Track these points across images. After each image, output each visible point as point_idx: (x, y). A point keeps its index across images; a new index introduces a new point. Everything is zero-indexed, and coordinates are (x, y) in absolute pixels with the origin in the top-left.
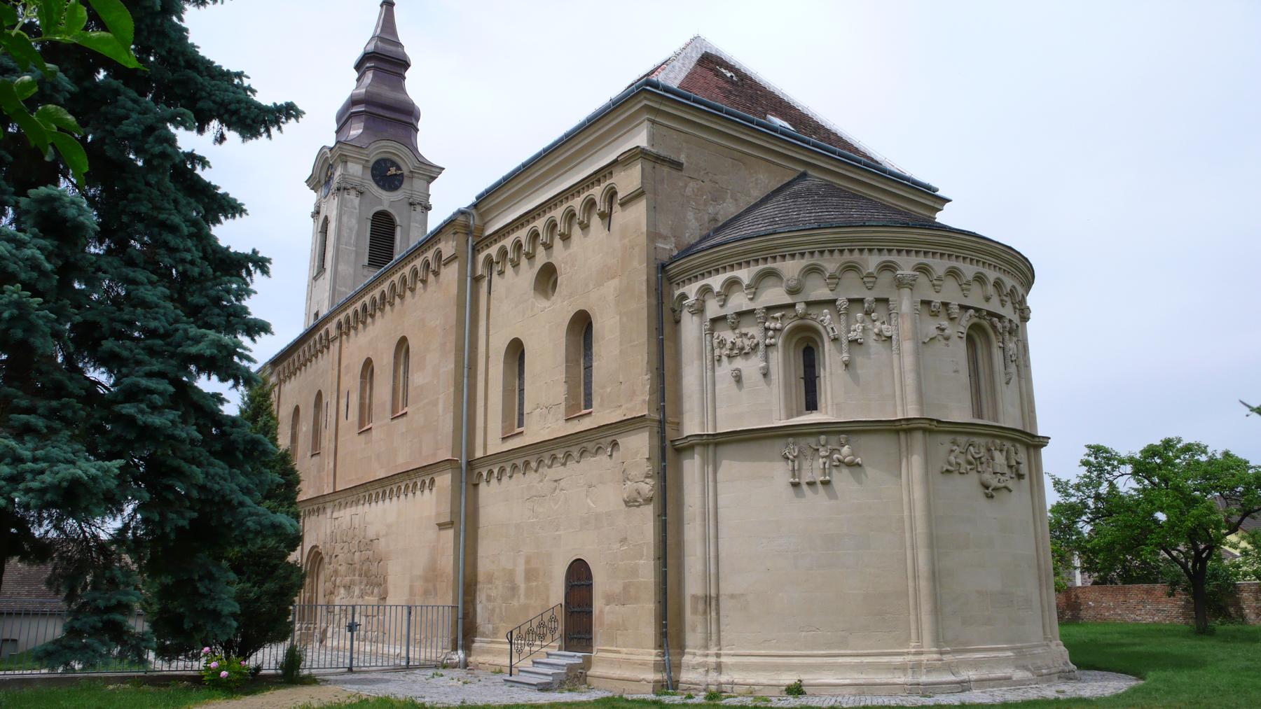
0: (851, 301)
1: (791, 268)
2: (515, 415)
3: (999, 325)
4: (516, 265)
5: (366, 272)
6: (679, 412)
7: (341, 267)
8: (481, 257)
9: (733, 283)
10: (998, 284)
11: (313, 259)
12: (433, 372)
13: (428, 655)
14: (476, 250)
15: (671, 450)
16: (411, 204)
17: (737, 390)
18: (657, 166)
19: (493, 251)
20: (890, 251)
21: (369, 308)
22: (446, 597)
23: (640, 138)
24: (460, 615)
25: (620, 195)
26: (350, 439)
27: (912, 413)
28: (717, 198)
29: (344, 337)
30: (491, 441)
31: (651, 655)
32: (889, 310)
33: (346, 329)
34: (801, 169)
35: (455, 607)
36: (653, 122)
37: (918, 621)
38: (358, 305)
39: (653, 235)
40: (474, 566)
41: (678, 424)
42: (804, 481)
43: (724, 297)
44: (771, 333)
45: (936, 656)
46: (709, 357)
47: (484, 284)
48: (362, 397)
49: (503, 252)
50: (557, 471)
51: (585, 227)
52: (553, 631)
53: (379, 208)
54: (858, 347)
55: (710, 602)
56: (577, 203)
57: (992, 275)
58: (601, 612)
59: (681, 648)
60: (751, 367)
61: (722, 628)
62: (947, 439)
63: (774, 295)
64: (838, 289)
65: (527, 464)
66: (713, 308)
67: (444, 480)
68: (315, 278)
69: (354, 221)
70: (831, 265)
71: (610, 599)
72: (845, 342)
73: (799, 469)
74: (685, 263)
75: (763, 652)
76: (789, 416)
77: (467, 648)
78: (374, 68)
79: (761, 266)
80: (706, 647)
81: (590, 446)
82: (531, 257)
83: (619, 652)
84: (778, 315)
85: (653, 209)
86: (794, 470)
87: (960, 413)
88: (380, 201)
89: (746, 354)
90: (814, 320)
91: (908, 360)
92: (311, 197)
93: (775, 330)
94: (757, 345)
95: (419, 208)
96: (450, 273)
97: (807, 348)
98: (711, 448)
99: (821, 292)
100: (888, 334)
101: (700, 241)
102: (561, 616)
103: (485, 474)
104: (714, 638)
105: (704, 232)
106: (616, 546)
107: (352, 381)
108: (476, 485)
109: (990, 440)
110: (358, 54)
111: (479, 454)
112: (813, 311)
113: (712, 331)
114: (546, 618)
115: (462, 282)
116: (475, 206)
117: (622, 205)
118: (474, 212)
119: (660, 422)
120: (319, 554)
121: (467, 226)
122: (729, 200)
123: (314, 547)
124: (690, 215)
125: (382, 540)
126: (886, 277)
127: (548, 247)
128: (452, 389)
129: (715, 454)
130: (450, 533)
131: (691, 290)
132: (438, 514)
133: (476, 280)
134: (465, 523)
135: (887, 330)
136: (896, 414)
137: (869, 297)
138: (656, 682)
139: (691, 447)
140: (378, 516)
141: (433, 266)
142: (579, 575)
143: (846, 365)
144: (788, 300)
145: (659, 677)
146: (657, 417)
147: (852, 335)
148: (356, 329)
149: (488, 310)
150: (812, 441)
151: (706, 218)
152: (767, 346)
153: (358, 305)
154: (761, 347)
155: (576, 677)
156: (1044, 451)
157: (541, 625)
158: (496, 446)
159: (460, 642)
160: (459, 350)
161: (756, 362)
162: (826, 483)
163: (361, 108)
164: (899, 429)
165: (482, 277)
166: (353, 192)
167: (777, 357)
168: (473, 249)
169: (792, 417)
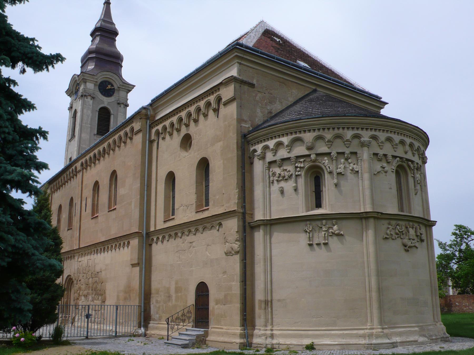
0: (338, 153)
1: (308, 137)
2: (170, 210)
5: (95, 137)
6: (252, 209)
8: (154, 130)
9: (279, 144)
10: (411, 145)
11: (69, 131)
12: (129, 188)
14: (151, 127)
16: (118, 104)
17: (281, 198)
18: (242, 86)
19: (160, 127)
20: (358, 128)
22: (135, 301)
25: (224, 100)
26: (87, 222)
29: (85, 170)
30: (158, 222)
31: (238, 330)
33: (85, 166)
34: (314, 88)
35: (140, 306)
36: (240, 64)
39: (240, 120)
41: (252, 214)
43: (275, 151)
44: (298, 169)
46: (268, 181)
47: (155, 144)
49: (165, 128)
50: (191, 238)
52: (189, 318)
53: (102, 106)
55: (268, 303)
56: (202, 104)
58: (213, 308)
59: (253, 326)
60: (288, 186)
61: (274, 316)
62: (386, 222)
63: (300, 150)
65: (176, 234)
66: (270, 157)
68: (70, 141)
69: (90, 112)
70: (328, 135)
71: (217, 302)
73: (313, 237)
74: (256, 134)
77: (146, 327)
79: (294, 136)
80: (266, 326)
82: (179, 130)
83: (222, 329)
84: (302, 160)
85: (240, 107)
86: (310, 237)
89: (286, 179)
91: (367, 183)
93: (301, 168)
94: (292, 175)
95: (122, 106)
96: (138, 138)
98: (268, 227)
102: (193, 310)
104: (269, 321)
105: (265, 119)
107: (88, 192)
108: (151, 245)
109: (407, 223)
111: (152, 229)
112: (320, 159)
114: (186, 311)
118: (150, 108)
121: (146, 115)
122: (278, 103)
123: (68, 276)
124: (258, 110)
125: (103, 272)
126: (356, 141)
127: (187, 126)
128: (139, 197)
130: (137, 269)
131: (259, 148)
132: (131, 259)
133: (151, 142)
135: (356, 168)
137: (347, 151)
138: (241, 343)
139: (259, 226)
140: (101, 260)
143: (336, 185)
144: (307, 153)
145: (242, 341)
146: (241, 211)
147: (339, 170)
148: (90, 166)
151: (266, 111)
153: (92, 154)
154: (294, 176)
156: (434, 228)
158: (161, 225)
159: (142, 324)
160: (142, 177)
162: (326, 244)
164: (362, 217)
165: (154, 140)
166: (89, 98)
167: (301, 181)
168: (150, 126)
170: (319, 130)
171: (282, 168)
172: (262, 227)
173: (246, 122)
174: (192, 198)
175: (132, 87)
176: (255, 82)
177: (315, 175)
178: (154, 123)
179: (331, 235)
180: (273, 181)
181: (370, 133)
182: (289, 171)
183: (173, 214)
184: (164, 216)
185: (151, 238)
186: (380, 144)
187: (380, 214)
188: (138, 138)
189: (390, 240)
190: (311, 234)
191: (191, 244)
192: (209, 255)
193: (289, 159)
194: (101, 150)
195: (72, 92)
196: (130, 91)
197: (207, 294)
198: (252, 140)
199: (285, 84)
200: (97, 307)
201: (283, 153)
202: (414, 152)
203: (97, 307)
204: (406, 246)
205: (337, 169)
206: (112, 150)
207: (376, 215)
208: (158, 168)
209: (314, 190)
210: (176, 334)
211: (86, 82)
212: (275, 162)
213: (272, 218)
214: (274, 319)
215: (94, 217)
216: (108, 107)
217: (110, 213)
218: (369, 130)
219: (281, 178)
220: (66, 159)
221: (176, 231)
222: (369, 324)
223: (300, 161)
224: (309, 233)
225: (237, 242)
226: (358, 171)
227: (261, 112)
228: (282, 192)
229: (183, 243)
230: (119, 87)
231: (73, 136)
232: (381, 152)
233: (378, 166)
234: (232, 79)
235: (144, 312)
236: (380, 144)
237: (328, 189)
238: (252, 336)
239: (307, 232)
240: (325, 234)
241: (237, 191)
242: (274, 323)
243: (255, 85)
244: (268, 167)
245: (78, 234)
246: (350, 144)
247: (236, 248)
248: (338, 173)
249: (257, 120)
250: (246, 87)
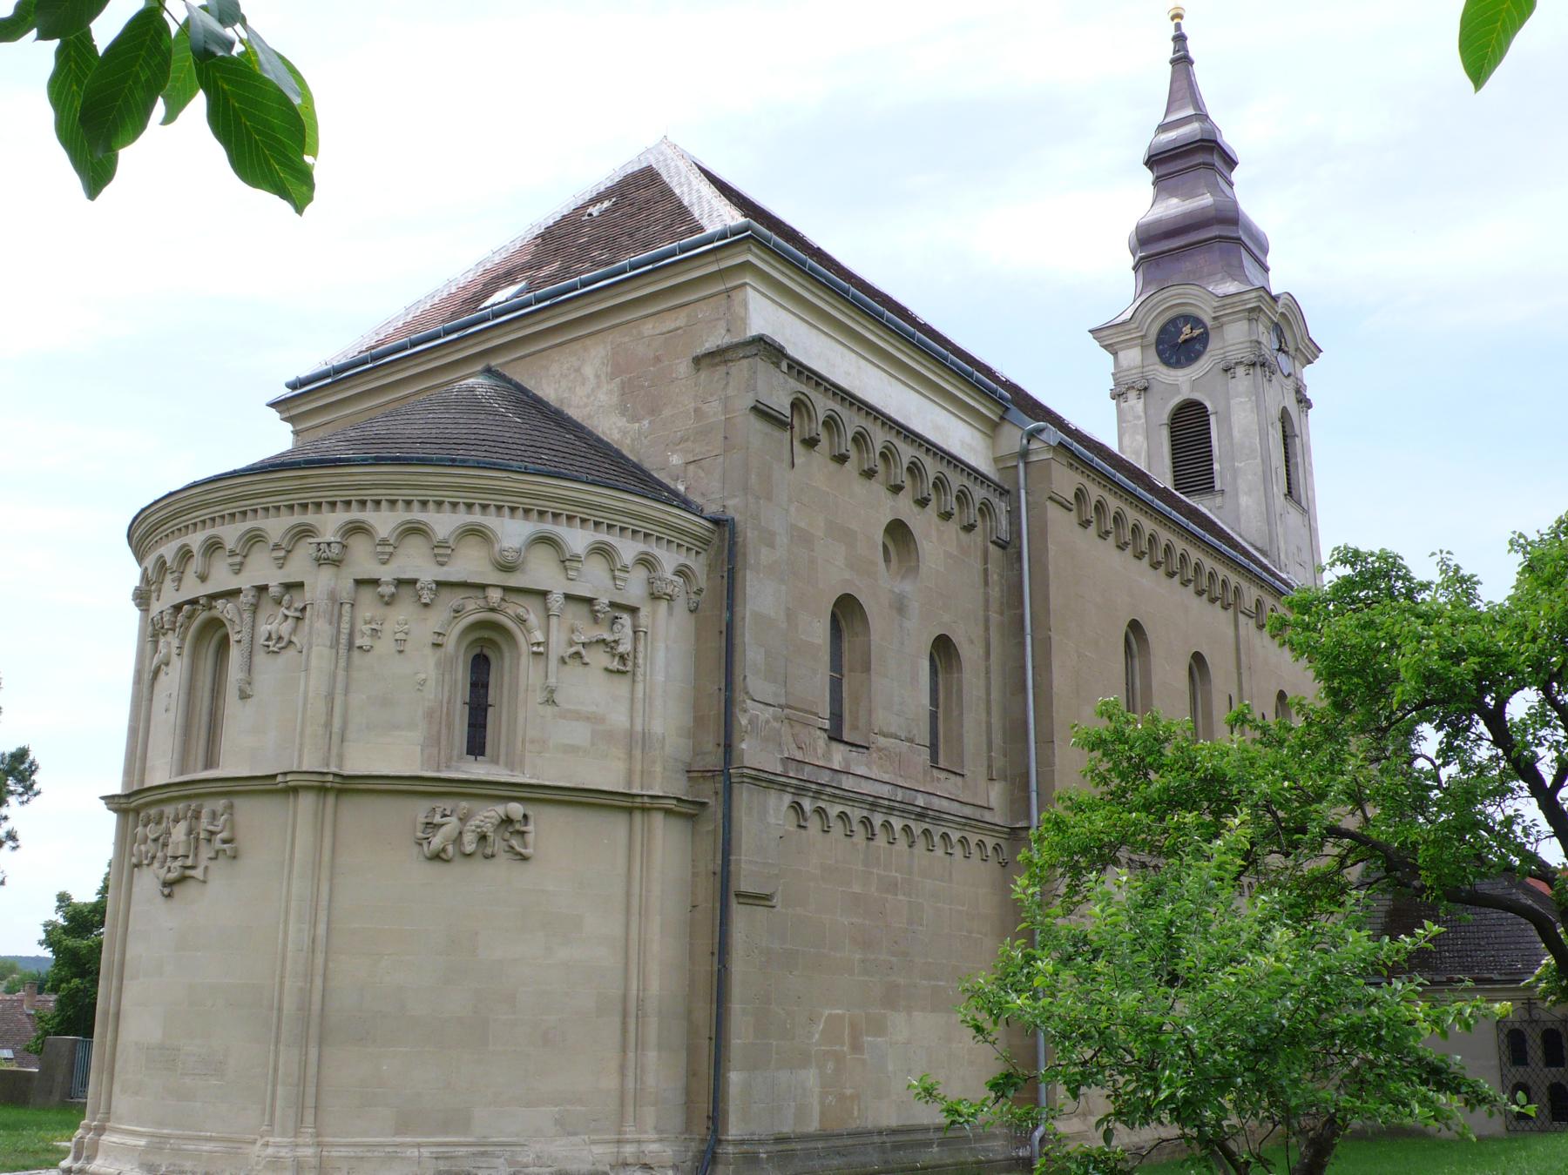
9: (254, 538)
32: (547, 609)
53: (1176, 401)
54: (581, 669)
63: (470, 564)
88: (1175, 388)
97: (484, 655)
98: (331, 799)
126: (359, 545)
129: (336, 805)
170: (469, 506)
177: (477, 651)
186: (230, 560)
201: (415, 563)
216: (1197, 396)
232: (387, 573)
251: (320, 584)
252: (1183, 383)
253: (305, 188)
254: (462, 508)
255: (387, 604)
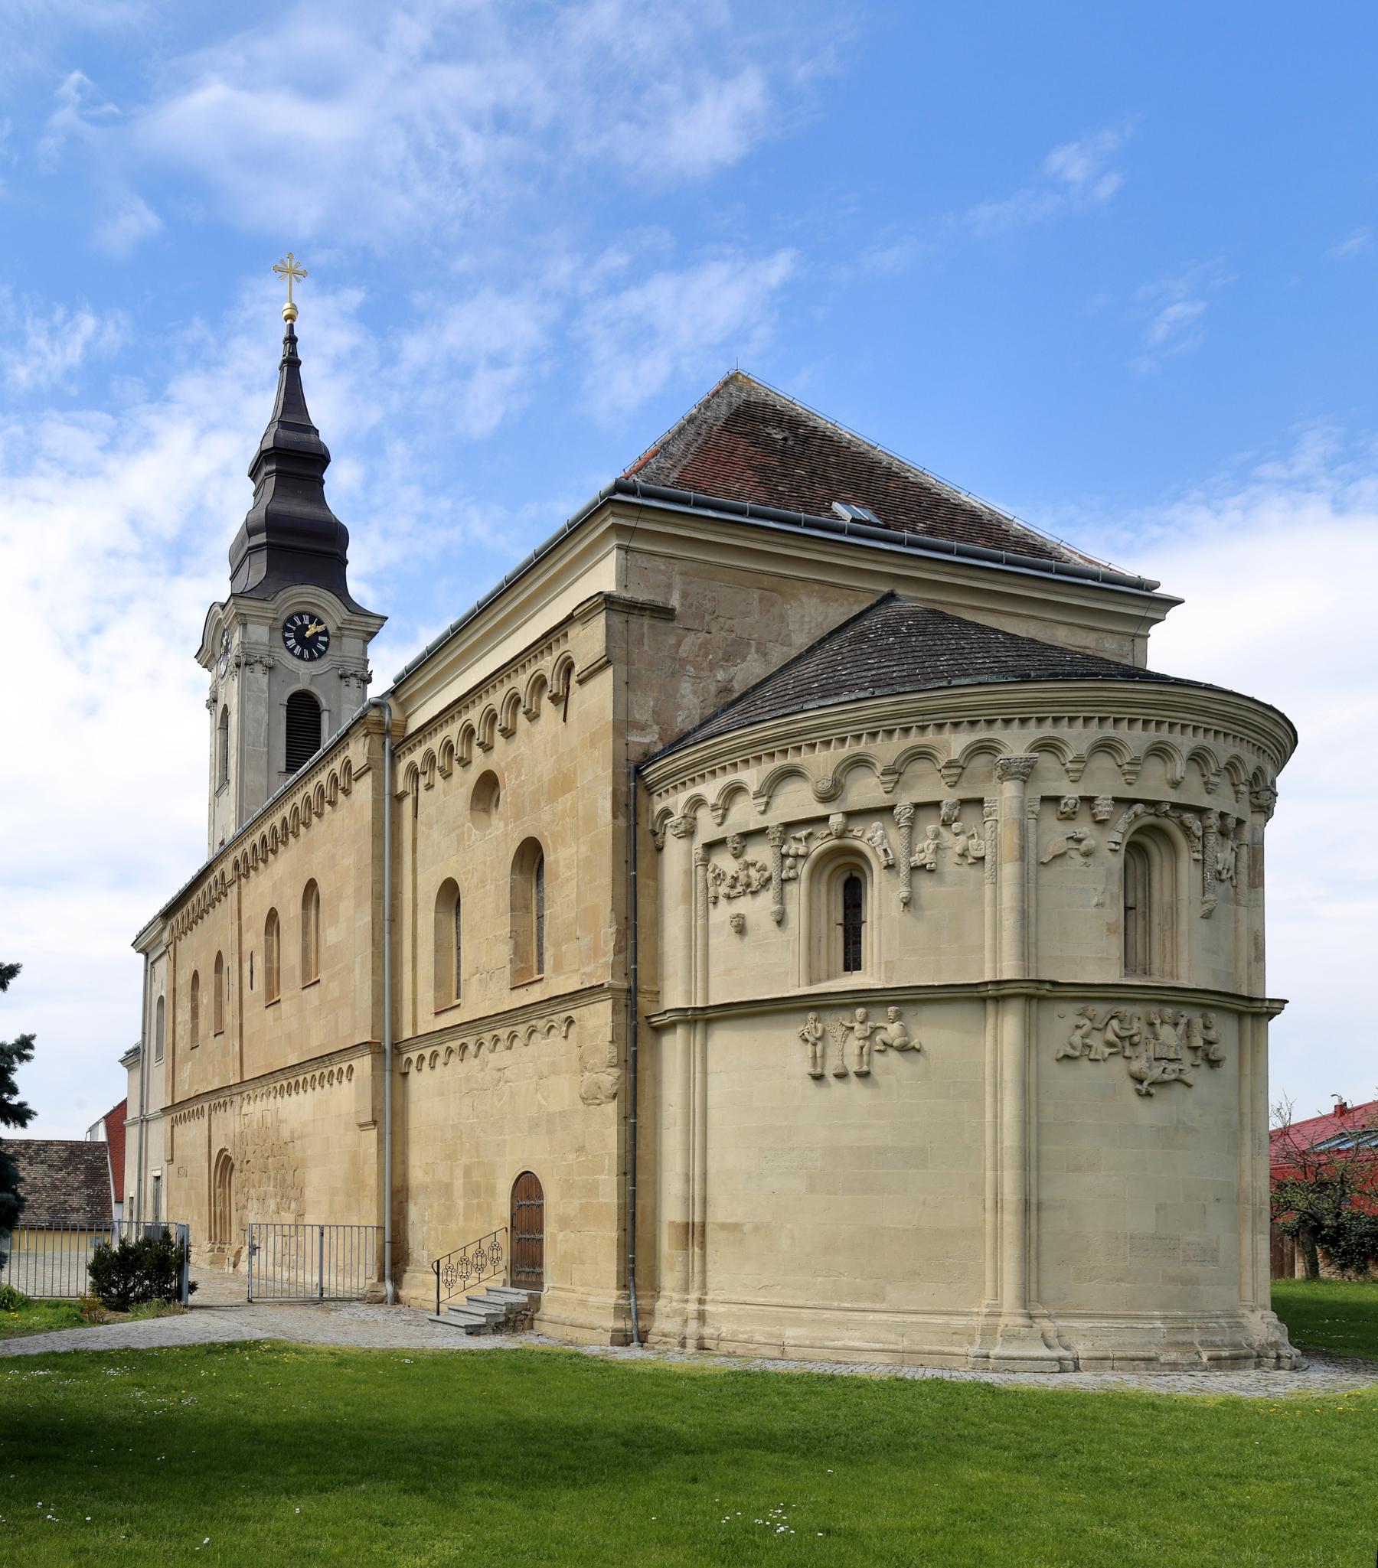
0: (918, 806)
1: (821, 762)
2: (449, 985)
3: (1196, 826)
4: (447, 775)
5: (283, 778)
6: (657, 977)
7: (249, 777)
8: (402, 766)
9: (735, 791)
10: (1198, 757)
11: (213, 767)
12: (347, 925)
13: (354, 1284)
14: (395, 757)
15: (640, 1026)
16: (341, 677)
17: (739, 941)
18: (633, 619)
19: (417, 756)
20: (990, 722)
21: (269, 841)
22: (369, 1213)
23: (603, 575)
24: (388, 1238)
25: (577, 669)
26: (257, 1017)
27: (1009, 970)
28: (733, 653)
29: (243, 880)
30: (421, 1015)
31: (609, 1295)
33: (245, 870)
34: (885, 588)
35: (380, 1228)
36: (627, 550)
37: (997, 1270)
38: (256, 838)
39: (623, 725)
40: (405, 1176)
41: (658, 993)
42: (829, 1072)
43: (724, 808)
44: (789, 861)
45: (1020, 1321)
46: (700, 899)
47: (408, 803)
48: (268, 959)
49: (430, 758)
50: (500, 1057)
51: (533, 716)
52: (495, 1261)
55: (693, 1233)
56: (521, 682)
57: (1185, 742)
58: (554, 1236)
59: (655, 1290)
60: (759, 908)
61: (709, 1266)
62: (1070, 1010)
63: (797, 801)
64: (898, 789)
65: (464, 1047)
66: (708, 828)
67: (363, 1064)
68: (217, 794)
69: (262, 710)
70: (886, 750)
71: (564, 1222)
72: (904, 870)
73: (823, 1056)
74: (666, 765)
75: (762, 1300)
76: (811, 983)
77: (397, 1280)
78: (277, 471)
79: (779, 762)
80: (686, 1289)
81: (541, 1024)
82: (465, 763)
83: (574, 1291)
84: (802, 833)
85: (625, 687)
86: (815, 1057)
87: (1101, 966)
88: (294, 676)
89: (753, 893)
90: (855, 837)
91: (1009, 893)
92: (207, 677)
93: (797, 856)
94: (769, 879)
95: (353, 682)
96: (363, 789)
98: (700, 1027)
99: (865, 790)
100: (980, 854)
101: (701, 726)
102: (504, 1240)
103: (415, 1059)
104: (697, 1280)
105: (709, 712)
106: (571, 1156)
107: (254, 939)
108: (405, 1075)
109: (1154, 1009)
110: (253, 453)
111: (407, 1034)
112: (857, 828)
113: (706, 861)
114: (486, 1245)
115: (377, 803)
116: (393, 692)
117: (581, 682)
118: (391, 702)
119: (629, 991)
120: (228, 1159)
121: (380, 723)
122: (753, 655)
123: (222, 1150)
124: (686, 687)
125: (298, 1143)
127: (487, 747)
128: (369, 951)
130: (372, 1134)
131: (677, 801)
132: (357, 1112)
133: (398, 798)
134: (390, 1120)
135: (976, 847)
136: (982, 973)
137: (948, 797)
138: (615, 1331)
139: (672, 1026)
140: (296, 1109)
141: (341, 783)
142: (527, 1188)
143: (905, 904)
144: (821, 810)
145: (620, 1325)
146: (623, 984)
147: (917, 859)
148: (256, 869)
149: (415, 840)
150: (844, 1018)
151: (713, 689)
152: (783, 881)
153: (256, 838)
154: (774, 883)
155: (516, 1320)
156: (1273, 1024)
157: (479, 1253)
158: (428, 1023)
159: (387, 1272)
160: (377, 896)
161: (766, 901)
162: (863, 1075)
163: (261, 538)
164: (985, 996)
165: (405, 794)
166: (258, 668)
167: (798, 893)
168: (393, 755)
169: (820, 981)
171: (741, 860)
172: (680, 1031)
173: (642, 728)
174: (503, 952)
175: (378, 622)
176: (675, 602)
177: (846, 876)
178: (401, 742)
179: (879, 1051)
180: (716, 898)
181: (1034, 733)
182: (764, 869)
183: (458, 997)
184: (436, 999)
185: (405, 1057)
187: (1048, 986)
188: (363, 789)
189: (1085, 1063)
190: (819, 1048)
191: (500, 1074)
192: (543, 1102)
193: (761, 832)
194: (278, 825)
195: (213, 655)
196: (373, 635)
197: (538, 1202)
198: (659, 782)
199: (780, 593)
200: (286, 1228)
201: (745, 814)
202: (1213, 779)
203: (286, 1228)
204: (1141, 1081)
205: (911, 853)
206: (304, 824)
207: (1031, 991)
208: (419, 870)
209: (841, 921)
210: (460, 1301)
211: (245, 625)
212: (721, 843)
213: (712, 1003)
214: (709, 1274)
215: (272, 1003)
216: (314, 689)
217: (307, 991)
218: (1033, 723)
219: (740, 889)
220: (211, 845)
221: (464, 1040)
222: (986, 1302)
223: (795, 838)
224: (815, 1045)
225: (610, 1070)
226: (983, 858)
227: (695, 692)
228: (741, 928)
229: (482, 1070)
230: (339, 628)
231: (225, 780)
232: (1071, 792)
233: (1054, 834)
234: (607, 602)
235: (392, 1242)
236: (1069, 765)
237: (880, 917)
238: (651, 1313)
239: (807, 1041)
240: (862, 1048)
241: (613, 929)
242: (709, 1285)
243: (674, 610)
244: (702, 859)
245: (237, 1048)
246: (960, 775)
247: (608, 1085)
248: (912, 868)
249: (679, 719)
250: (645, 624)
251: (1005, 796)
252: (304, 674)
253: (312, 436)
254: (1033, 723)
255: (1068, 819)
